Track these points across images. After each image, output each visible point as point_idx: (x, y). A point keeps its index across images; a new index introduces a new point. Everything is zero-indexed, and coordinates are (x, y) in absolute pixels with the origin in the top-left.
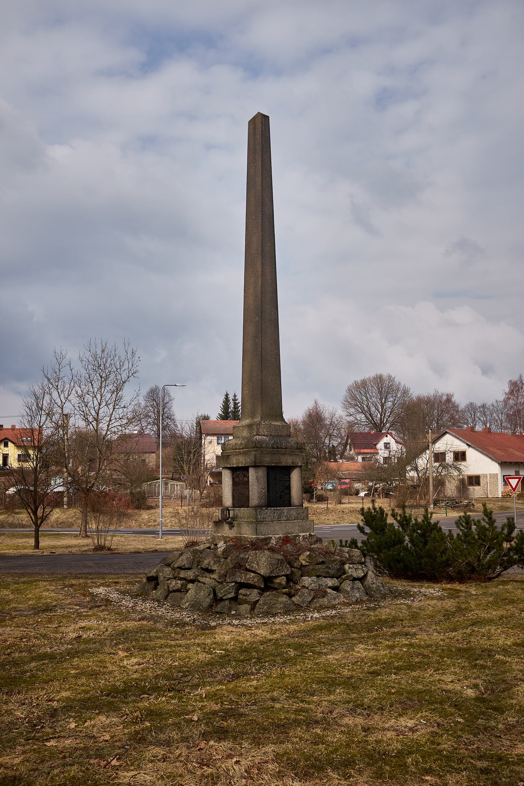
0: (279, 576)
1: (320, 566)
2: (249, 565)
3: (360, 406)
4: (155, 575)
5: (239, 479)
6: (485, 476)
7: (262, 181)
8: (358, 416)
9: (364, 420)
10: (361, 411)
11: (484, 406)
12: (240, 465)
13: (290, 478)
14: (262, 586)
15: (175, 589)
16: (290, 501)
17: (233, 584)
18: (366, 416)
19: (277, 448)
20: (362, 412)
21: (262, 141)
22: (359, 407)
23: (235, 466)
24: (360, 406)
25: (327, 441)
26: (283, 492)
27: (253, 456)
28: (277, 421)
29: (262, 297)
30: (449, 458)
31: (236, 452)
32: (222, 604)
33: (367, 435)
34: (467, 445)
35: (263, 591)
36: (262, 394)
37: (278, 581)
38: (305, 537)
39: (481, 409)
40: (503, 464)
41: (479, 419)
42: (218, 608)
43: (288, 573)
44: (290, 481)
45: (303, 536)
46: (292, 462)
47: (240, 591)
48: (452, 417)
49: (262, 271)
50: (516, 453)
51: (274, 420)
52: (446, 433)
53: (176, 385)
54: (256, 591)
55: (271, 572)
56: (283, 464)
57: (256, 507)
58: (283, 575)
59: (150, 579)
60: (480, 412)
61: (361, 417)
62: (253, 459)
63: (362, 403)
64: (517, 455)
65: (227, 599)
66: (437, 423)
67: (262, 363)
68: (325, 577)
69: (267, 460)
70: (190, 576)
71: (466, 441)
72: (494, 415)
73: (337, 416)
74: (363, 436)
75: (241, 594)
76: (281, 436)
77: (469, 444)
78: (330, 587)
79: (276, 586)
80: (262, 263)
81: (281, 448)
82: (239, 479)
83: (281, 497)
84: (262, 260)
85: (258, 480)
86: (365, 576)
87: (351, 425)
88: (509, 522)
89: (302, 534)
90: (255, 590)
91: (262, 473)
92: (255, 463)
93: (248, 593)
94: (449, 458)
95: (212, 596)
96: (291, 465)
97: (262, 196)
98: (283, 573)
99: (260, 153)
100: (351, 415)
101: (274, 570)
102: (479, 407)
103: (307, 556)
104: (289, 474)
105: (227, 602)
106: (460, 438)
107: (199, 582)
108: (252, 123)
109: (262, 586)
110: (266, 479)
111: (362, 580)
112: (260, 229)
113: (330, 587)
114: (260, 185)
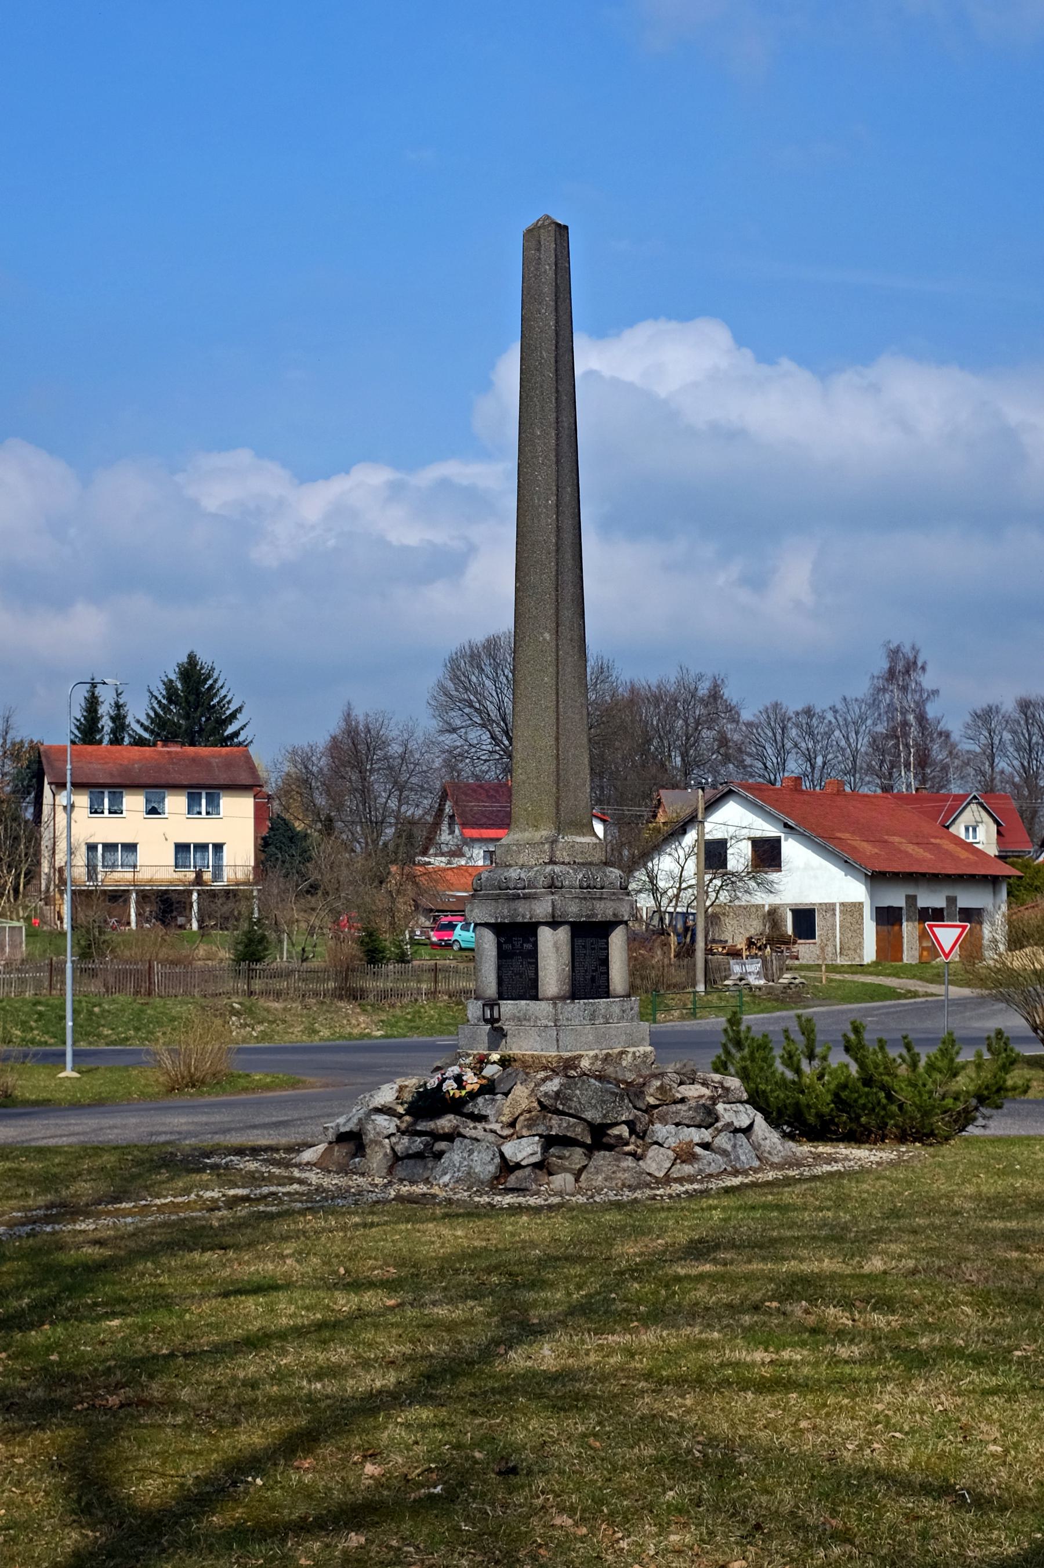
0: (617, 1124)
1: (679, 1106)
2: (563, 1105)
3: (477, 705)
4: (356, 1129)
5: (513, 946)
6: (830, 908)
7: (556, 362)
8: (474, 735)
9: (489, 747)
10: (478, 720)
11: (809, 712)
12: (520, 919)
13: (607, 943)
14: (589, 1141)
15: (411, 1152)
16: (608, 987)
17: (537, 1138)
18: (493, 737)
19: (588, 887)
20: (483, 726)
21: (556, 278)
22: (476, 709)
23: (506, 921)
24: (477, 705)
25: (393, 804)
26: (596, 970)
27: (550, 904)
28: (584, 835)
29: (557, 595)
30: (739, 856)
31: (507, 895)
32: (519, 1173)
33: (497, 791)
34: (786, 825)
35: (590, 1150)
36: (558, 784)
37: (615, 1131)
38: (637, 1054)
39: (803, 720)
40: (876, 878)
41: (796, 745)
42: (512, 1180)
43: (631, 1118)
44: (607, 949)
45: (634, 1053)
46: (615, 915)
47: (552, 1150)
48: (723, 741)
49: (557, 544)
50: (910, 848)
51: (578, 834)
52: (730, 793)
53: (104, 683)
54: (579, 1150)
55: (605, 1116)
56: (599, 918)
57: (554, 999)
58: (624, 1122)
59: (342, 1138)
60: (798, 726)
61: (479, 736)
62: (550, 910)
63: (481, 697)
64: (911, 855)
65: (528, 1165)
66: (684, 756)
67: (558, 724)
68: (688, 1126)
69: (573, 910)
70: (443, 1128)
71: (782, 816)
72: (837, 733)
73: (419, 734)
74: (487, 791)
75: (553, 1156)
76: (591, 864)
77: (791, 823)
78: (697, 1144)
79: (612, 1141)
80: (558, 527)
81: (595, 887)
82: (513, 946)
83: (593, 979)
84: (558, 521)
85: (557, 949)
86: (751, 1125)
87: (453, 759)
88: (655, 1011)
89: (631, 1050)
90: (578, 1149)
91: (563, 934)
92: (553, 917)
93: (567, 1154)
94: (739, 856)
95: (497, 1160)
96: (613, 919)
97: (557, 391)
98: (624, 1118)
99: (552, 303)
100: (454, 730)
101: (608, 1112)
102: (797, 714)
103: (657, 1088)
104: (607, 936)
105: (528, 1171)
106: (768, 808)
107: (464, 1137)
108: (532, 235)
109: (589, 1141)
110: (569, 946)
111: (748, 1130)
112: (554, 459)
113: (697, 1144)
114: (553, 369)
